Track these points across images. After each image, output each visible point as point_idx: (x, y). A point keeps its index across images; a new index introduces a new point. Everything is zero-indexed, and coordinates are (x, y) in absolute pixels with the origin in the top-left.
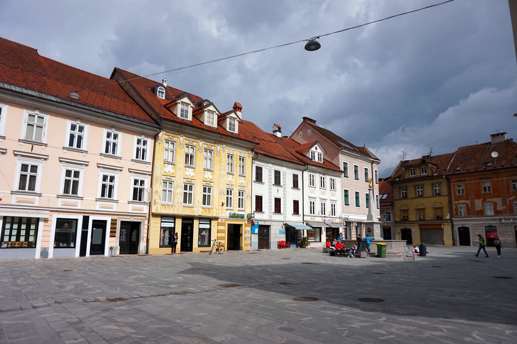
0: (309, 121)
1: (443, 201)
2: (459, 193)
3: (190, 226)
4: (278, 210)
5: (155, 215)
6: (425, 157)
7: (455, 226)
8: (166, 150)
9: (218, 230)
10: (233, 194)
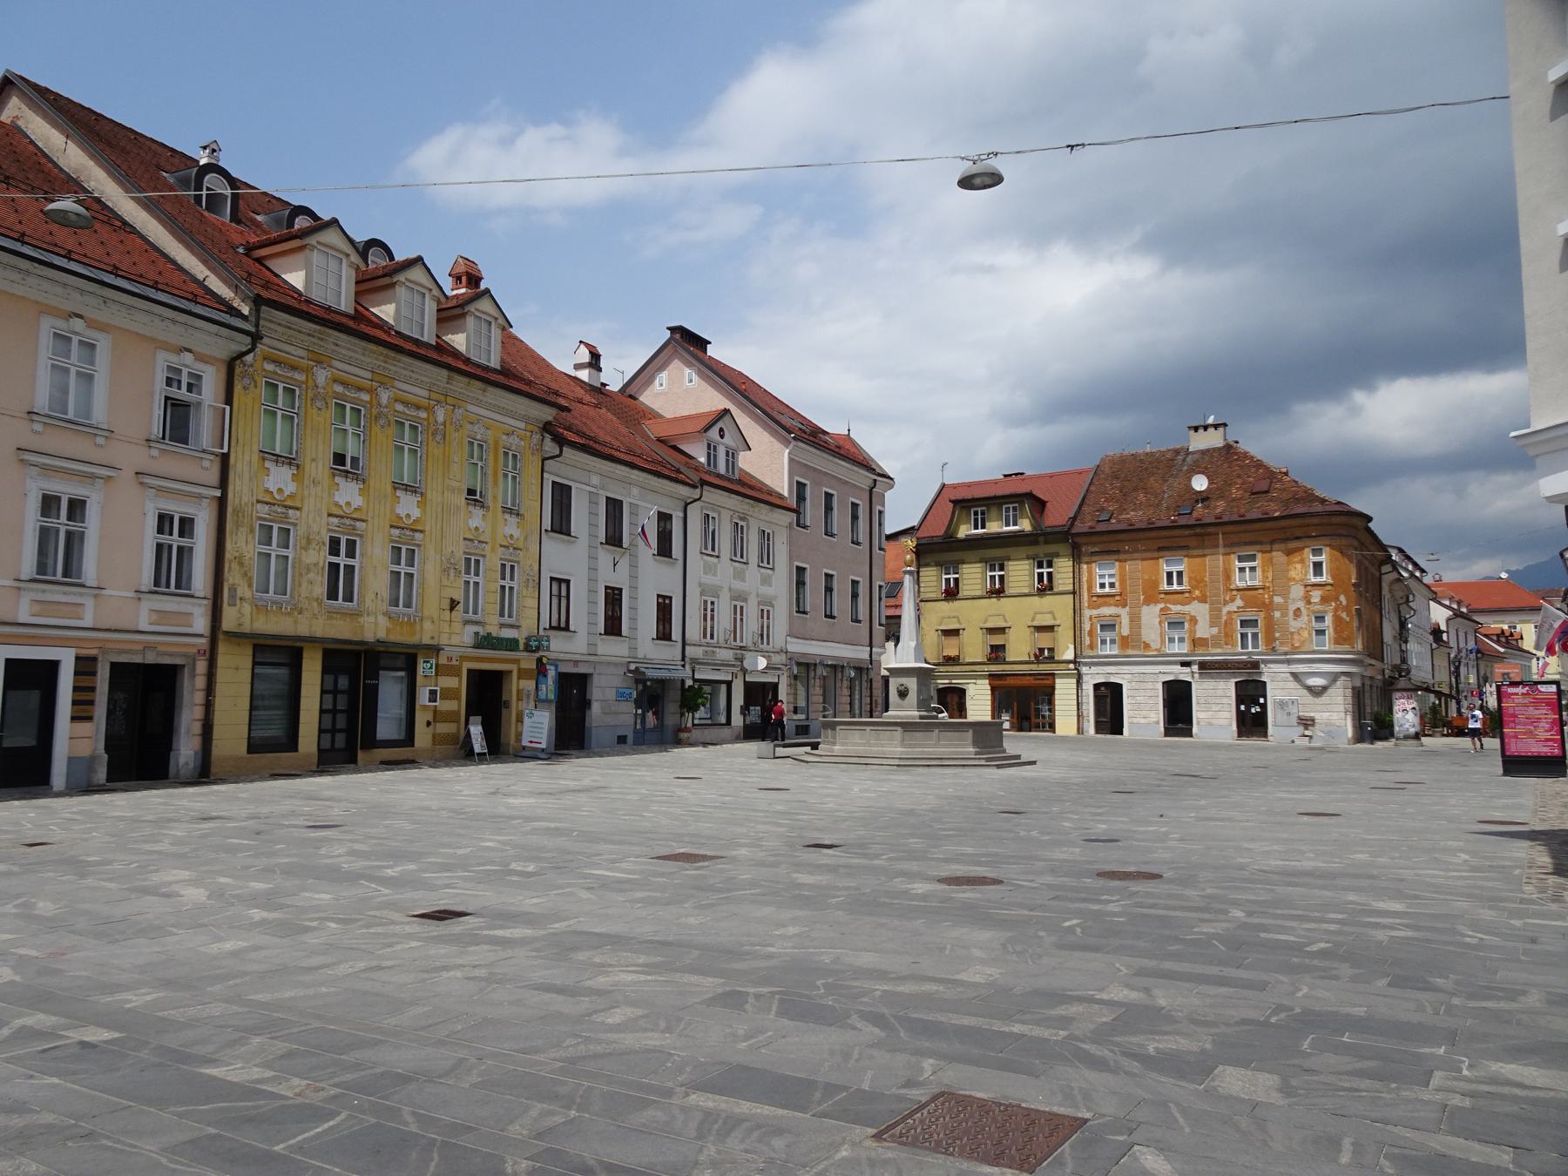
2: (1170, 582)
4: (613, 627)
7: (1085, 678)
10: (485, 572)
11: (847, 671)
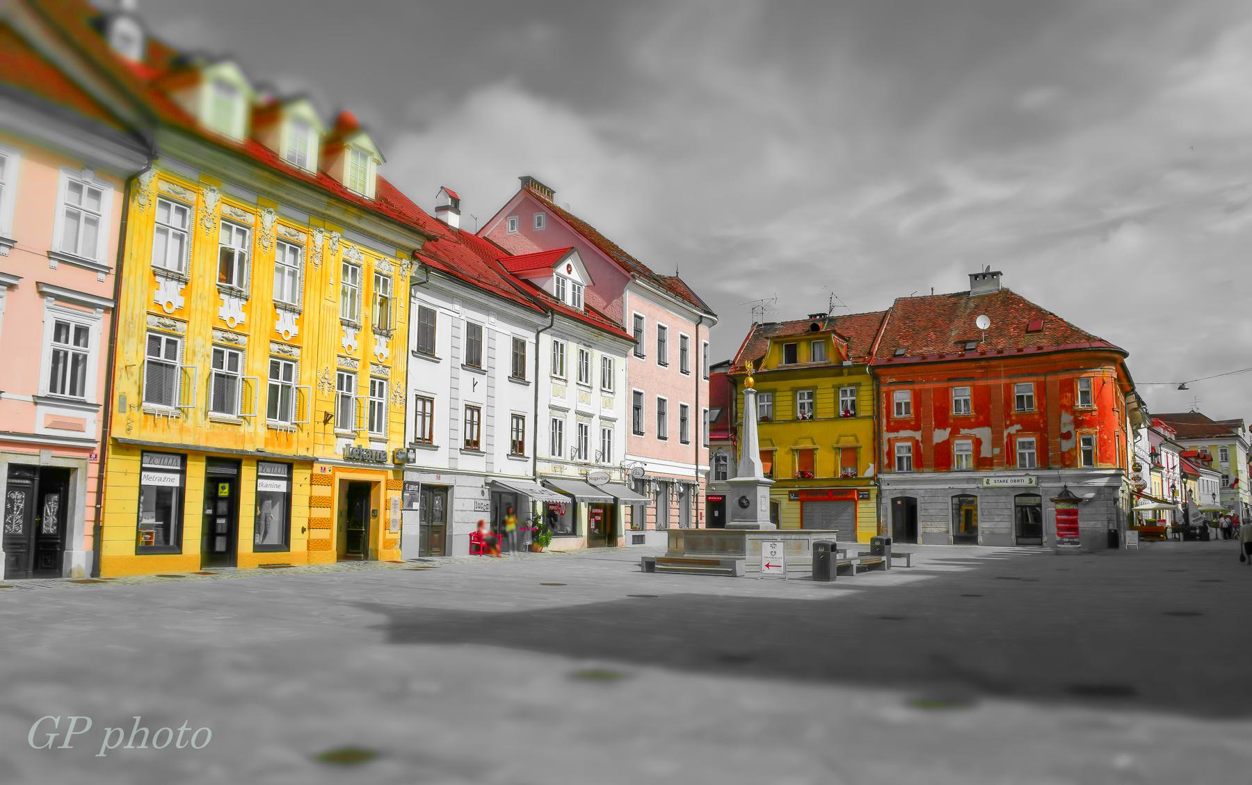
1: (859, 432)
2: (899, 413)
3: (227, 485)
5: (124, 447)
6: (815, 316)
7: (884, 494)
8: (159, 230)
9: (311, 498)
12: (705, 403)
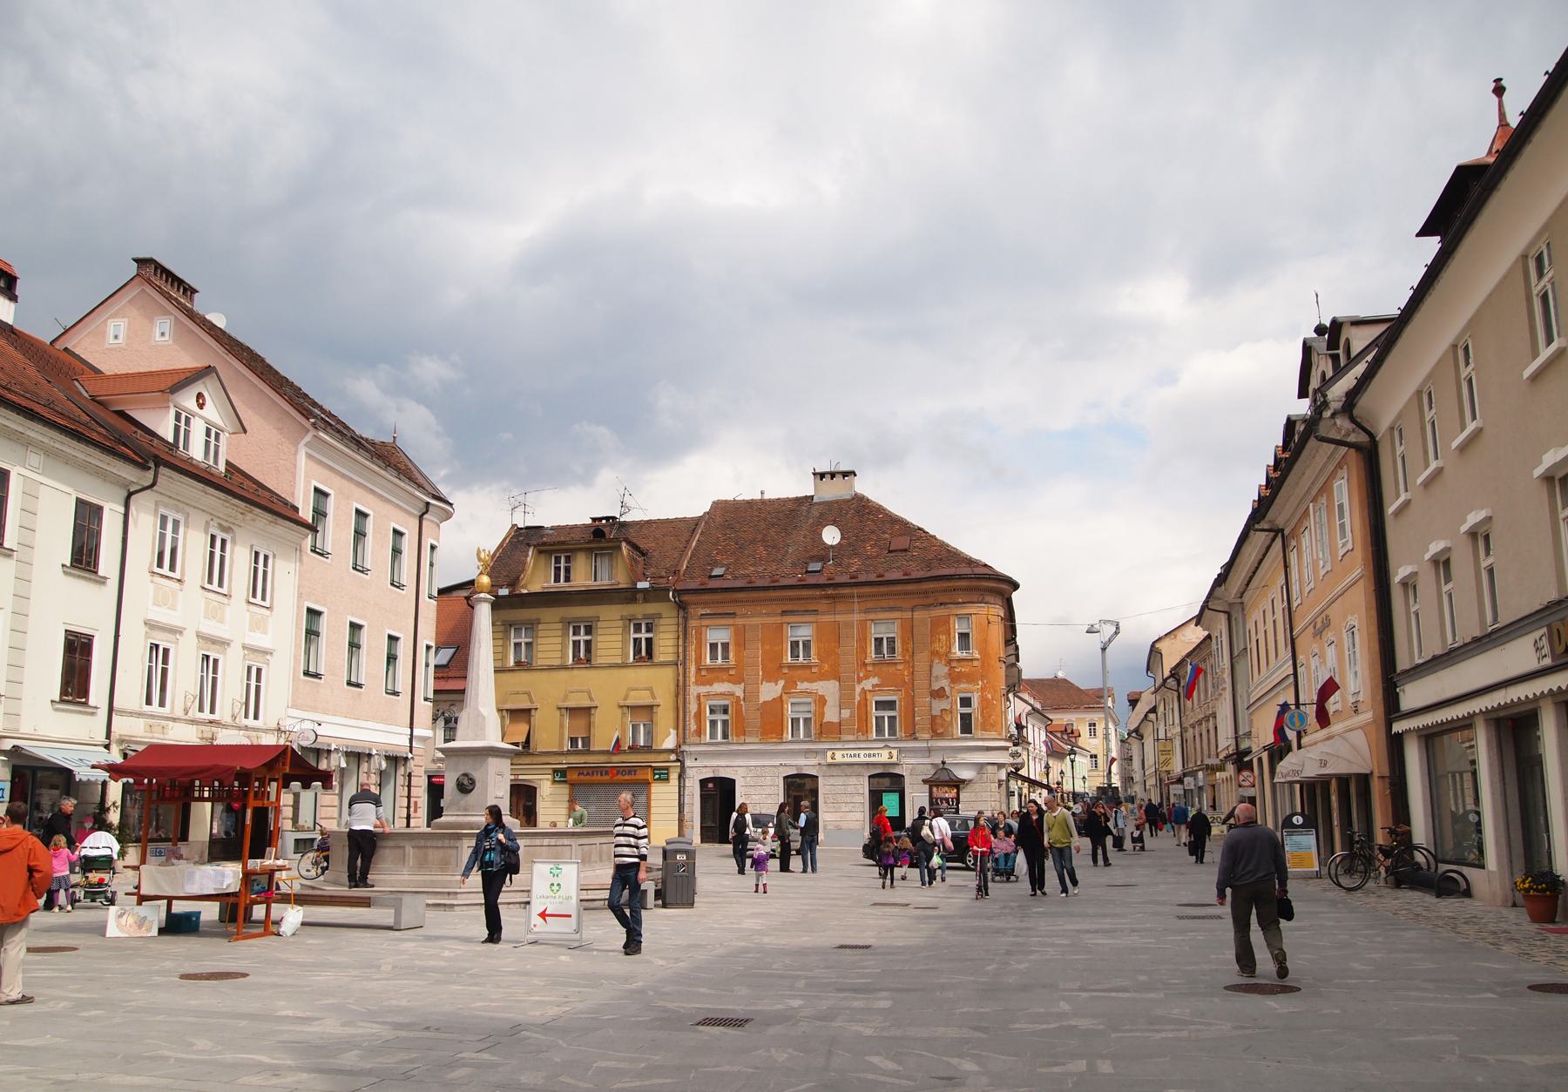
0: (167, 281)
6: (600, 519)
7: (689, 772)
11: (334, 756)
12: (428, 636)
